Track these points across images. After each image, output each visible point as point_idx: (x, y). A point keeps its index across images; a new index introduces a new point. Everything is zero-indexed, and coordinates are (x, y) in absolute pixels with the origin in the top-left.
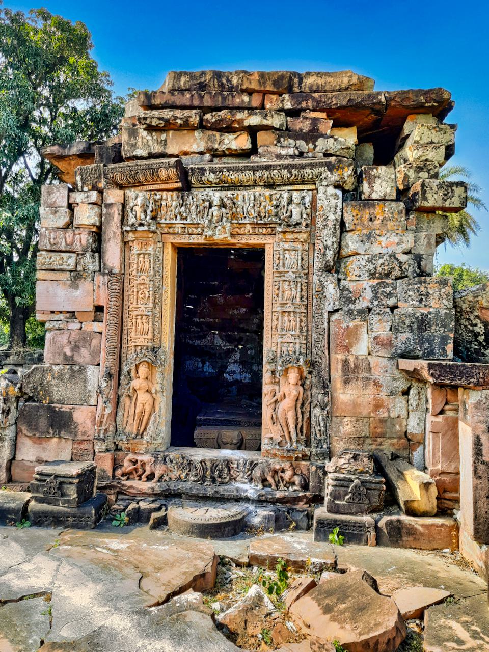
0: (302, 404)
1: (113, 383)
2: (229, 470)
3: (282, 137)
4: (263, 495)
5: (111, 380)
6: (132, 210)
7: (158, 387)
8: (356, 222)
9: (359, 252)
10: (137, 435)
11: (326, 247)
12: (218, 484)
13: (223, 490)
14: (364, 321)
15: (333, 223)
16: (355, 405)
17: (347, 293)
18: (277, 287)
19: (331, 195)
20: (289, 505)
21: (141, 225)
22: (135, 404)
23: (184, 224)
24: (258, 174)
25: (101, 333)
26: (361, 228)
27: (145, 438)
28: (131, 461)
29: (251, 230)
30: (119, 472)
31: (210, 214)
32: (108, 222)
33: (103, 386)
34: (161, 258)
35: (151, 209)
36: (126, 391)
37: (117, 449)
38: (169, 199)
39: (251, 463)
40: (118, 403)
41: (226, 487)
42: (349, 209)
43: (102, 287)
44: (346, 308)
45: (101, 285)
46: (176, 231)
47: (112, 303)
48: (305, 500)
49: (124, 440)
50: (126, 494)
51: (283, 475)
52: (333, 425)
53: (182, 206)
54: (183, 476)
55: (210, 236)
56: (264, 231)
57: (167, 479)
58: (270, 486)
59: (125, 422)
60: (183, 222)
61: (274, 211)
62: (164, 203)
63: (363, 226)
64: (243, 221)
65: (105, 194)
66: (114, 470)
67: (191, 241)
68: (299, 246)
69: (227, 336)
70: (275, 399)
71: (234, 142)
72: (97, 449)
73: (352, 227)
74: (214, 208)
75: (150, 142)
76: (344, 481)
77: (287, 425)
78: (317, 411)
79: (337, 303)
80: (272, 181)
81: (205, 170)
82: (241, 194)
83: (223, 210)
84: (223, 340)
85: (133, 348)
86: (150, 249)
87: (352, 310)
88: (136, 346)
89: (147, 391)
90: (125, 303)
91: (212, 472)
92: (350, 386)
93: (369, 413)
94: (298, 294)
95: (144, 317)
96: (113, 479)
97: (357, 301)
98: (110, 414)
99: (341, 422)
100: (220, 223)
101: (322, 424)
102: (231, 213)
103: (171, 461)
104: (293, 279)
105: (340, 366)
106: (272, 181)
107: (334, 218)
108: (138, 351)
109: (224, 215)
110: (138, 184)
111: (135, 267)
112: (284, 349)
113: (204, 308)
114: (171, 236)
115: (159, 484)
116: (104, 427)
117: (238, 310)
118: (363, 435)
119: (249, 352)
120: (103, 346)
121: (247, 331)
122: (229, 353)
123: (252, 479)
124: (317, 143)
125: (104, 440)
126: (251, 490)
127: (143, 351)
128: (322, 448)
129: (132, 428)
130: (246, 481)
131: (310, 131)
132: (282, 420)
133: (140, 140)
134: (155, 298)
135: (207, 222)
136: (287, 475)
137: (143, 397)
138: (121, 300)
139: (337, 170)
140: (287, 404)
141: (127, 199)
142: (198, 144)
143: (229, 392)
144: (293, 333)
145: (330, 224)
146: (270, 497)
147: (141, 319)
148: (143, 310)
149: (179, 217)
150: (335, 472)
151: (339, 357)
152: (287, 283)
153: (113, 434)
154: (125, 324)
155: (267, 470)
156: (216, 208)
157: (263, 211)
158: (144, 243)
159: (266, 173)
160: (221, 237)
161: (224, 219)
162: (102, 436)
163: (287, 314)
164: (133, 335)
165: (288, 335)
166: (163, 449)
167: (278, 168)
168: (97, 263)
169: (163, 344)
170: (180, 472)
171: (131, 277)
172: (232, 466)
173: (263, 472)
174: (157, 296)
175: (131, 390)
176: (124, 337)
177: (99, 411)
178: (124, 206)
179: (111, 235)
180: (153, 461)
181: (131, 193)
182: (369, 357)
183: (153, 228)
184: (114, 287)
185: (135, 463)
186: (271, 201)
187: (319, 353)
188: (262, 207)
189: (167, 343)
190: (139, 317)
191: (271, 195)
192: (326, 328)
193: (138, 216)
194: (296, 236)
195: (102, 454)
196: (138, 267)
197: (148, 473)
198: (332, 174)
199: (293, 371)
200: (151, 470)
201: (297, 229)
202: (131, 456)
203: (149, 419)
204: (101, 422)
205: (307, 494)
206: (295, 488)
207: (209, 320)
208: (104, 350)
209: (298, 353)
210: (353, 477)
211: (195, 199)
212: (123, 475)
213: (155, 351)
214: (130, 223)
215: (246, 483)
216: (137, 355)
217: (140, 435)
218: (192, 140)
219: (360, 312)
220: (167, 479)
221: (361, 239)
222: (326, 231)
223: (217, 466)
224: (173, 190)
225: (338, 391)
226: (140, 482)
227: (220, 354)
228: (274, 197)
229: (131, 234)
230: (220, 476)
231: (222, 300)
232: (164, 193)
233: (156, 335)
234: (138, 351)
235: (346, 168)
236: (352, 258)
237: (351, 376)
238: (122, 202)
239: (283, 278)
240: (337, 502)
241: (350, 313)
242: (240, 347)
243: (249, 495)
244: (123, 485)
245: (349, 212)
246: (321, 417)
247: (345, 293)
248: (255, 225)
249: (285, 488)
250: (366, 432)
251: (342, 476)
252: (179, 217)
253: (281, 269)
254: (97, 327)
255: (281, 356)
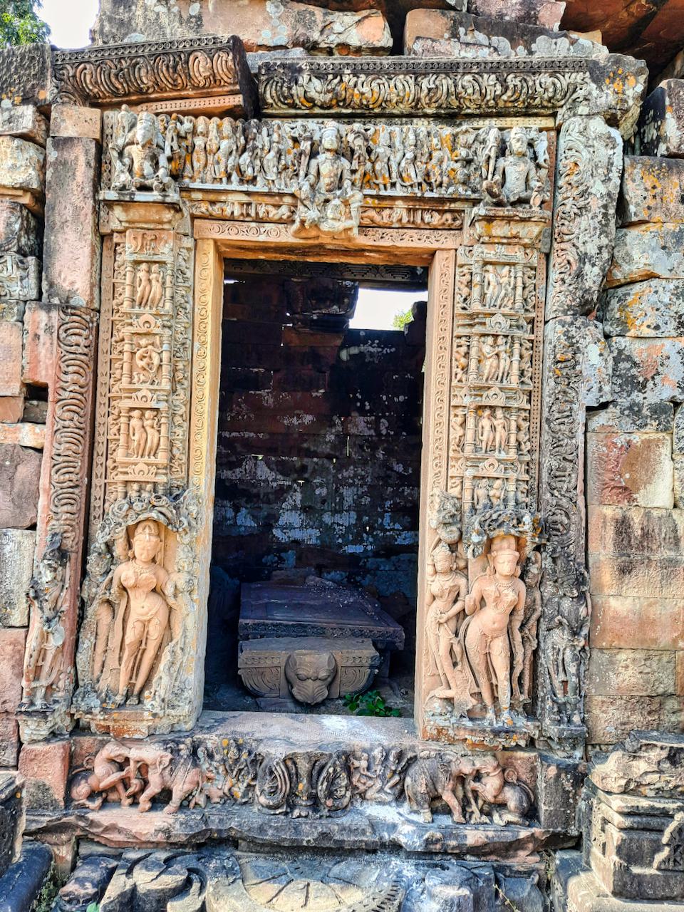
0: (526, 623)
1: (70, 572)
2: (350, 775)
3: (461, 24)
4: (438, 841)
5: (64, 565)
6: (121, 154)
7: (181, 579)
8: (651, 202)
9: (657, 271)
10: (127, 697)
11: (583, 258)
12: (325, 812)
13: (337, 827)
14: (666, 429)
15: (601, 203)
16: (644, 622)
17: (628, 365)
18: (464, 349)
19: (600, 137)
20: (494, 858)
21: (144, 188)
22: (124, 621)
23: (248, 193)
24: (426, 83)
25: (40, 451)
26: (663, 218)
27: (148, 703)
28: (111, 761)
29: (405, 214)
30: (81, 790)
31: (313, 171)
32: (61, 182)
33: (45, 579)
34: (189, 274)
35: (168, 152)
36: (101, 590)
37: (79, 728)
38: (213, 134)
39: (400, 756)
40: (82, 617)
41: (346, 820)
42: (638, 171)
43: (44, 338)
44: (624, 401)
45: (41, 333)
46: (228, 211)
47: (69, 378)
48: (531, 846)
49: (96, 711)
50: (98, 843)
51: (477, 785)
52: (593, 669)
53: (244, 150)
54: (239, 790)
55: (315, 225)
56: (436, 219)
57: (201, 800)
58: (448, 811)
59: (98, 666)
60: (245, 188)
61: (461, 172)
62: (199, 142)
63: (667, 213)
64: (389, 192)
65: (53, 115)
66: (70, 782)
67: (262, 238)
68: (517, 254)
69: (277, 463)
70: (458, 607)
71: (354, 31)
72: (26, 734)
73: (643, 215)
74: (321, 157)
75: (164, 20)
76: (648, 815)
77: (490, 669)
78: (559, 638)
79: (607, 388)
80: (455, 103)
81: (300, 70)
82: (382, 131)
83: (345, 163)
84: (272, 470)
85: (120, 488)
86: (165, 251)
87: (638, 405)
88: (126, 483)
89: (154, 590)
90: (100, 379)
91: (312, 783)
92: (631, 580)
93: (675, 641)
94: (515, 365)
95: (148, 414)
96: (66, 807)
97: (650, 384)
98: (60, 650)
99: (611, 662)
100: (338, 192)
101: (572, 669)
102: (361, 171)
103: (210, 756)
104: (505, 332)
105: (610, 533)
106: (455, 103)
107: (604, 191)
108: (133, 494)
109: (347, 174)
110: (139, 98)
111: (128, 293)
112: (481, 492)
113: (238, 414)
114: (216, 224)
115: (182, 817)
116: (44, 682)
117: (299, 418)
118: (660, 690)
119: (317, 492)
120: (44, 481)
121: (315, 454)
122: (281, 493)
123: (402, 791)
124: (534, 47)
125: (43, 714)
126: (406, 824)
127: (145, 495)
128: (569, 721)
129: (116, 679)
130: (389, 798)
131: (521, 19)
132: (477, 661)
133: (139, 12)
134: (175, 370)
135: (306, 187)
136: (489, 787)
137: (142, 606)
138: (90, 372)
139: (613, 82)
140: (489, 620)
141: (108, 131)
142: (273, 28)
143: (281, 560)
144: (503, 456)
145: (595, 204)
146: (453, 843)
147: (142, 418)
148: (145, 395)
149: (235, 177)
150: (624, 793)
151: (609, 512)
152: (490, 340)
153: (69, 696)
154: (100, 430)
155: (442, 777)
156: (329, 155)
157: (437, 170)
158: (152, 233)
159: (446, 83)
160: (340, 226)
161: (347, 184)
162: (39, 703)
163: (487, 412)
164: (120, 455)
165: (491, 460)
166: (190, 725)
167: (475, 70)
168: (32, 280)
169: (194, 479)
170: (230, 781)
171: (116, 317)
172: (357, 763)
173: (433, 781)
174: (180, 366)
175: (115, 589)
176: (98, 460)
177: (32, 643)
178: (100, 148)
179: (68, 213)
180: (166, 761)
181: (119, 117)
182: (676, 514)
183: (173, 196)
184: (74, 339)
185: (122, 765)
186: (453, 149)
187: (564, 502)
188: (434, 161)
189: (203, 477)
190: (136, 413)
191: (455, 136)
192: (582, 446)
193: (136, 166)
194: (515, 229)
195: (39, 747)
196: (134, 291)
197: (153, 789)
198: (600, 88)
199: (505, 544)
200: (163, 782)
201: (521, 212)
202: (112, 750)
203: (157, 657)
204: (38, 669)
205: (537, 830)
206: (509, 817)
207: (247, 435)
208: (47, 492)
209: (512, 503)
210: (671, 806)
211: (275, 137)
212: (92, 795)
213: (174, 494)
214: (116, 183)
215: (389, 803)
216: (131, 504)
217: (135, 695)
218: (260, 19)
219: (658, 410)
220: (201, 800)
221: (662, 243)
222: (584, 222)
223: (322, 768)
224: (223, 114)
225: (606, 591)
226: (134, 812)
227: (266, 494)
228: (462, 139)
229: (118, 212)
230: (330, 794)
231: (271, 401)
232: (201, 122)
233: (177, 457)
234: (133, 494)
235: (631, 79)
236: (637, 287)
237: (636, 556)
238: (98, 136)
239: (478, 329)
240: (636, 870)
241: (634, 410)
242: (301, 482)
243: (403, 840)
244: (92, 823)
245: (637, 178)
246: (568, 652)
247: (622, 365)
248: (416, 203)
249: (485, 819)
250: (667, 685)
251: (644, 803)
252: (235, 177)
253: (476, 307)
254: (29, 434)
255: (474, 509)
